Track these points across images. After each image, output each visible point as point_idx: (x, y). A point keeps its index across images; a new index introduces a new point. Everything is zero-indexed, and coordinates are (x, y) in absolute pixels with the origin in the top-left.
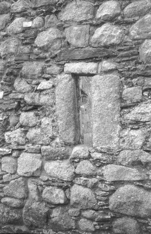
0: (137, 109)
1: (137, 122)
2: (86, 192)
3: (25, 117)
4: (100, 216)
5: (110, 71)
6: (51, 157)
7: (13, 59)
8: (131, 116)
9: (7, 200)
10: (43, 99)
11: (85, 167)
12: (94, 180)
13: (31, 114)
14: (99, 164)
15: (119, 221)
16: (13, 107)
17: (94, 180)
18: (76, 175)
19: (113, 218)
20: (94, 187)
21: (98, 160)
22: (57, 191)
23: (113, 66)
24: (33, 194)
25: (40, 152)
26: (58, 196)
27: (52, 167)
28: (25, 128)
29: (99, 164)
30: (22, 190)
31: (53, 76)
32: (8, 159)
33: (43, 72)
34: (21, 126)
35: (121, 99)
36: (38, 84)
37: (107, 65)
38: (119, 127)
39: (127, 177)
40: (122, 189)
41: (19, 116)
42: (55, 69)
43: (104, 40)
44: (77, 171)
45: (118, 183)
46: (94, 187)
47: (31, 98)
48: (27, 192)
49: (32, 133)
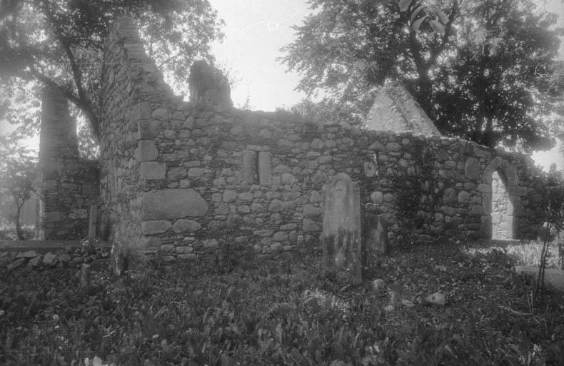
0: (277, 167)
1: (277, 173)
2: (259, 205)
3: (225, 171)
4: (265, 215)
5: (267, 151)
6: (241, 191)
7: (216, 138)
8: (275, 170)
9: (219, 217)
10: (236, 161)
11: (259, 194)
12: (262, 200)
13: (229, 169)
14: (265, 191)
15: (272, 216)
16: (41, 207)
17: (262, 200)
18: (254, 198)
19: (271, 214)
20: (262, 203)
21: (264, 190)
22: (246, 207)
23: (242, 184)
24: (234, 211)
25: (235, 189)
26: (246, 209)
27: (243, 196)
28: (226, 176)
29: (265, 191)
30: (227, 210)
31: (240, 150)
32: (218, 194)
33: (236, 147)
34: (223, 176)
35: (272, 163)
36: (232, 154)
37: (266, 148)
38: (271, 175)
39: (275, 196)
40: (273, 201)
41: (221, 170)
42: (243, 147)
43: (265, 136)
44: (255, 196)
45: (272, 199)
46: (262, 203)
47: (10, 216)
48: (229, 209)
49: (230, 180)
